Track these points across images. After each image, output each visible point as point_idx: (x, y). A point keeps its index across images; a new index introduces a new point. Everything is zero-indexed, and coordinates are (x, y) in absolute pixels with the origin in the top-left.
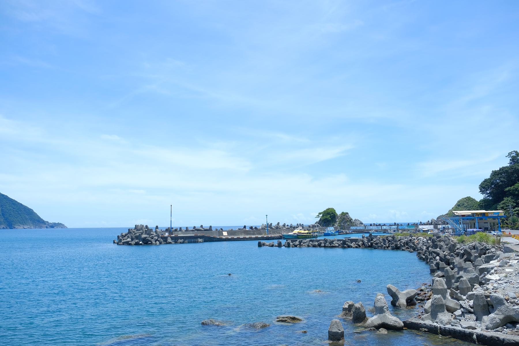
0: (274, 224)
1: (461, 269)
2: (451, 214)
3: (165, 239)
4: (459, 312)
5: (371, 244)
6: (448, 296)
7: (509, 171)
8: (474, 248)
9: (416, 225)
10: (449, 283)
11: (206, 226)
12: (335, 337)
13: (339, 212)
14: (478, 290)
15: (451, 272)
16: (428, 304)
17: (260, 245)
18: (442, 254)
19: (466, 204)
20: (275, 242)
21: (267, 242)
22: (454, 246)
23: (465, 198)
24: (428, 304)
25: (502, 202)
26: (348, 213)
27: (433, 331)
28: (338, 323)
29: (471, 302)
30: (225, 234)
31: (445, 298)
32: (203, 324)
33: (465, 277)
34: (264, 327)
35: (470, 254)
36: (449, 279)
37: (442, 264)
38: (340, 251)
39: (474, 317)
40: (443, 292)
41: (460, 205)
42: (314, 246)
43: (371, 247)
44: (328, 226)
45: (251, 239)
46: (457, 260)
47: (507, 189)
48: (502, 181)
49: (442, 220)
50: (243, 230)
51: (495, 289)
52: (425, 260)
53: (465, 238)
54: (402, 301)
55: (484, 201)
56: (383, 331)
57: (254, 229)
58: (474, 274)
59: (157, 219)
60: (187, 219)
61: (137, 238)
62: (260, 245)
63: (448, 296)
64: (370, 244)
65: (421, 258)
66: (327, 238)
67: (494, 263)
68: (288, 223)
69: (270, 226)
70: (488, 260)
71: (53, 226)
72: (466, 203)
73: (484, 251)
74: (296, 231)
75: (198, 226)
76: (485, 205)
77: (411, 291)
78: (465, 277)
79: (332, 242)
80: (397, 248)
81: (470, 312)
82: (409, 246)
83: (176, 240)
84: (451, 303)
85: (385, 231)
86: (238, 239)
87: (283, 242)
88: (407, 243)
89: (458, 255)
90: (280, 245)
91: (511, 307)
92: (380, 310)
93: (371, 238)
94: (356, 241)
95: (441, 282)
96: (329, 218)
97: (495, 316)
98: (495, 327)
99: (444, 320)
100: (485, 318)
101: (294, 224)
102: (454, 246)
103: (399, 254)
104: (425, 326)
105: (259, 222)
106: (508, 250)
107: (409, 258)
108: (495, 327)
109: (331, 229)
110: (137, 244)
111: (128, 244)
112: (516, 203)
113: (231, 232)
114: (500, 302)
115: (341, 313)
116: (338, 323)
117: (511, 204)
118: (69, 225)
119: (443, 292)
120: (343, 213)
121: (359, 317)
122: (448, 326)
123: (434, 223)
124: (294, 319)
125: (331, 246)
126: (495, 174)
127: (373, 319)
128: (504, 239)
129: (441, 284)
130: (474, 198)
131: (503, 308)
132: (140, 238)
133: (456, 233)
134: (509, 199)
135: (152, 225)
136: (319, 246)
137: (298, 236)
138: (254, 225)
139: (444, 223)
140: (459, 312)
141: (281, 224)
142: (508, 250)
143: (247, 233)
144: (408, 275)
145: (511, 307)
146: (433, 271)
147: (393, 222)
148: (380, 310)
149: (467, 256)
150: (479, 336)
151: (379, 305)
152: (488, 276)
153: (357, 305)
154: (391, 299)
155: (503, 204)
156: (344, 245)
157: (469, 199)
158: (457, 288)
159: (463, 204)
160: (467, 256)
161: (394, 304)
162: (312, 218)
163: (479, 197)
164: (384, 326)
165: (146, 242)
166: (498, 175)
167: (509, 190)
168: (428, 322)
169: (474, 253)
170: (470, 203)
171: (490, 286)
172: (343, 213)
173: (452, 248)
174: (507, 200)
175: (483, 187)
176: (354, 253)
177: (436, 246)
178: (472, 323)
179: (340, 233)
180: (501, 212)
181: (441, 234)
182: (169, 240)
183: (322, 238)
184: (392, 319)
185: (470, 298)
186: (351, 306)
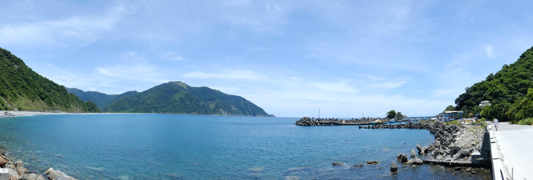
0: (367, 118)
1: (447, 136)
2: (444, 113)
3: (317, 123)
4: (445, 155)
5: (410, 126)
6: (441, 148)
8: (452, 127)
9: (430, 117)
10: (441, 143)
11: (335, 118)
12: (394, 170)
13: (396, 112)
14: (452, 145)
15: (443, 138)
16: (433, 153)
17: (360, 128)
18: (440, 130)
20: (367, 126)
21: (363, 126)
22: (444, 126)
24: (433, 153)
27: (435, 163)
28: (395, 163)
29: (449, 150)
30: (344, 122)
31: (439, 149)
32: (334, 164)
33: (448, 139)
34: (361, 166)
35: (450, 130)
36: (441, 141)
37: (440, 134)
38: (397, 130)
39: (450, 156)
40: (439, 147)
41: (448, 109)
43: (411, 128)
44: (391, 118)
45: (356, 125)
46: (445, 132)
49: (441, 115)
50: (352, 120)
51: (458, 143)
52: (432, 133)
53: (449, 123)
54: (423, 152)
55: (457, 107)
56: (414, 166)
57: (357, 120)
58: (451, 138)
59: (313, 115)
60: (326, 114)
61: (304, 122)
62: (360, 128)
63: (441, 148)
65: (431, 132)
66: (391, 124)
67: (458, 133)
68: (373, 117)
69: (365, 119)
70: (457, 131)
71: (270, 116)
72: (450, 108)
73: (455, 128)
74: (376, 121)
75: (331, 118)
76: (457, 109)
77: (426, 147)
78: (448, 139)
79: (393, 126)
80: (422, 128)
81: (449, 154)
82: (427, 127)
83: (321, 124)
84: (442, 151)
85: (417, 120)
86: (350, 125)
87: (371, 126)
88: (426, 126)
89: (446, 130)
90: (369, 128)
91: (463, 150)
92: (413, 157)
93: (411, 124)
94: (404, 125)
95: (438, 143)
96: (392, 115)
97: (458, 155)
98: (458, 159)
99: (439, 158)
100: (454, 156)
101: (376, 118)
102: (444, 126)
103: (422, 130)
104: (432, 162)
105: (360, 117)
106: (463, 127)
107: (426, 132)
108: (458, 159)
109: (393, 120)
110: (304, 125)
111: (300, 125)
113: (346, 121)
114: (459, 149)
115: (396, 159)
116: (395, 163)
117: (465, 108)
118: (277, 116)
119: (439, 147)
121: (404, 160)
122: (441, 161)
123: (437, 117)
124: (375, 162)
125: (392, 127)
126: (461, 96)
127: (410, 161)
128: (463, 123)
129: (438, 143)
131: (460, 151)
132: (306, 123)
133: (446, 121)
135: (311, 117)
136: (387, 127)
137: (377, 124)
138: (357, 118)
139: (441, 116)
140: (445, 155)
141: (370, 118)
142: (463, 127)
143: (354, 122)
144: (425, 139)
145: (463, 150)
146: (436, 138)
147: (420, 116)
148: (413, 157)
149: (449, 131)
150: (452, 163)
151: (413, 154)
152: (456, 139)
153: (403, 155)
154: (418, 151)
156: (399, 127)
157: (451, 106)
158: (445, 144)
160: (449, 131)
161: (419, 153)
162: (384, 115)
163: (455, 105)
164: (415, 163)
165: (308, 125)
168: (433, 160)
169: (452, 129)
171: (456, 143)
173: (444, 127)
175: (456, 101)
176: (403, 130)
177: (437, 127)
178: (449, 158)
179: (397, 122)
180: (462, 111)
181: (440, 122)
182: (318, 124)
183: (389, 124)
184: (418, 160)
185: (449, 148)
186: (401, 156)
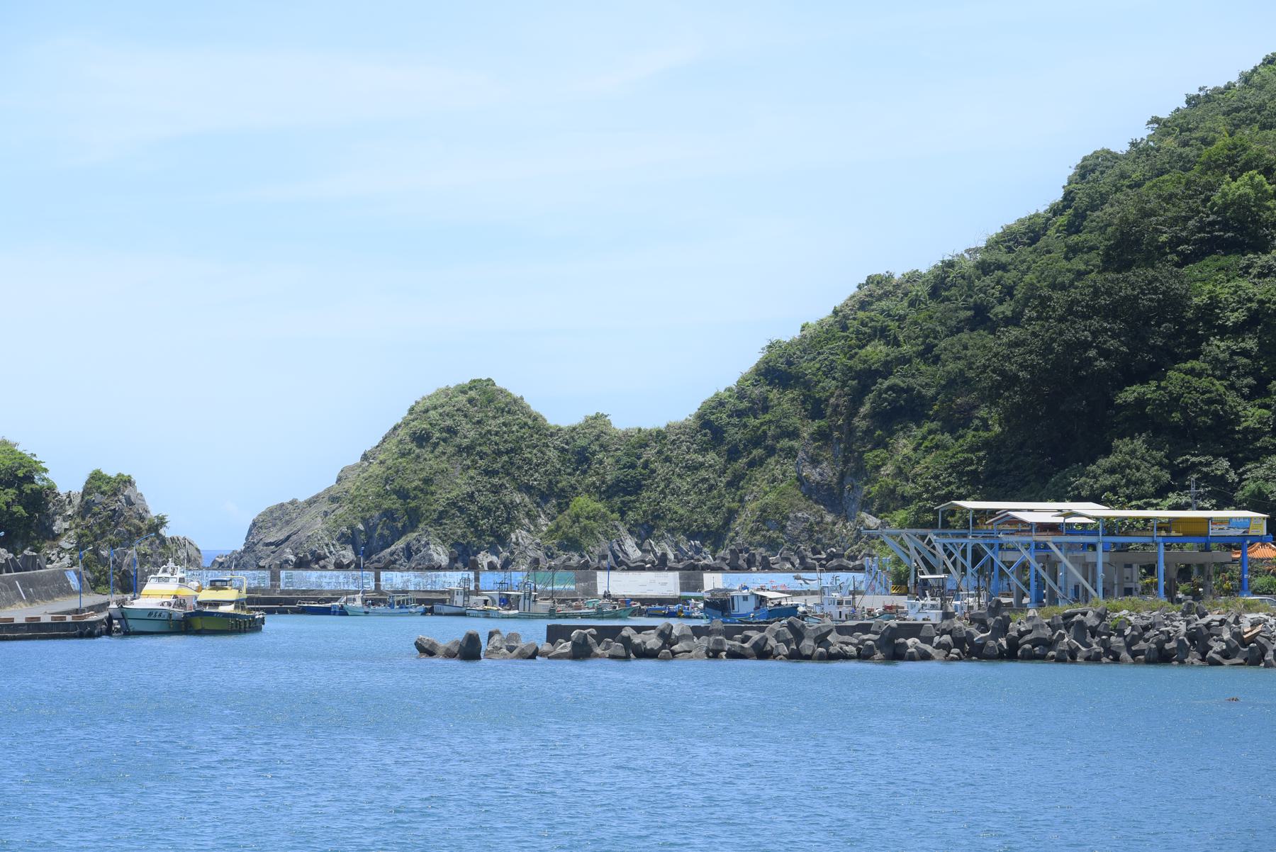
7: (1144, 302)
13: (67, 480)
19: (469, 433)
23: (463, 390)
25: (1104, 462)
26: (128, 482)
42: (733, 655)
47: (1130, 394)
48: (1105, 354)
64: (1003, 641)
80: (1162, 657)
112: (1170, 467)
120: (96, 477)
130: (516, 393)
134: (1139, 444)
155: (1112, 471)
159: (452, 431)
166: (1085, 317)
167: (1141, 402)
170: (493, 425)
172: (96, 477)
174: (1133, 453)
